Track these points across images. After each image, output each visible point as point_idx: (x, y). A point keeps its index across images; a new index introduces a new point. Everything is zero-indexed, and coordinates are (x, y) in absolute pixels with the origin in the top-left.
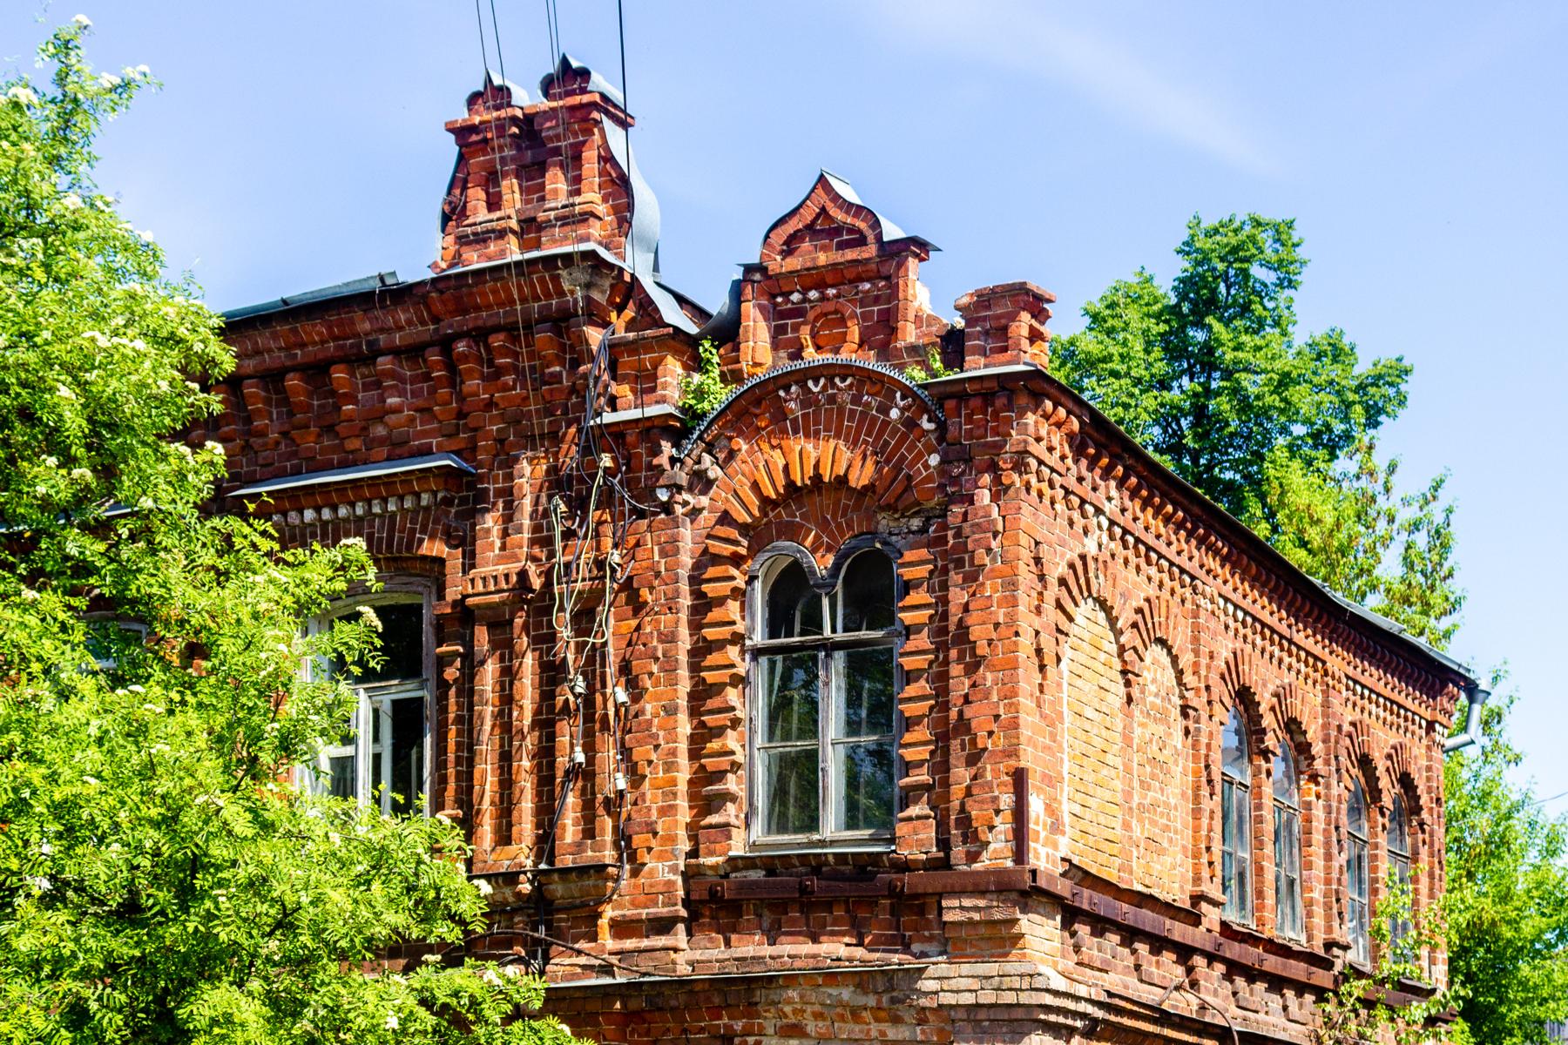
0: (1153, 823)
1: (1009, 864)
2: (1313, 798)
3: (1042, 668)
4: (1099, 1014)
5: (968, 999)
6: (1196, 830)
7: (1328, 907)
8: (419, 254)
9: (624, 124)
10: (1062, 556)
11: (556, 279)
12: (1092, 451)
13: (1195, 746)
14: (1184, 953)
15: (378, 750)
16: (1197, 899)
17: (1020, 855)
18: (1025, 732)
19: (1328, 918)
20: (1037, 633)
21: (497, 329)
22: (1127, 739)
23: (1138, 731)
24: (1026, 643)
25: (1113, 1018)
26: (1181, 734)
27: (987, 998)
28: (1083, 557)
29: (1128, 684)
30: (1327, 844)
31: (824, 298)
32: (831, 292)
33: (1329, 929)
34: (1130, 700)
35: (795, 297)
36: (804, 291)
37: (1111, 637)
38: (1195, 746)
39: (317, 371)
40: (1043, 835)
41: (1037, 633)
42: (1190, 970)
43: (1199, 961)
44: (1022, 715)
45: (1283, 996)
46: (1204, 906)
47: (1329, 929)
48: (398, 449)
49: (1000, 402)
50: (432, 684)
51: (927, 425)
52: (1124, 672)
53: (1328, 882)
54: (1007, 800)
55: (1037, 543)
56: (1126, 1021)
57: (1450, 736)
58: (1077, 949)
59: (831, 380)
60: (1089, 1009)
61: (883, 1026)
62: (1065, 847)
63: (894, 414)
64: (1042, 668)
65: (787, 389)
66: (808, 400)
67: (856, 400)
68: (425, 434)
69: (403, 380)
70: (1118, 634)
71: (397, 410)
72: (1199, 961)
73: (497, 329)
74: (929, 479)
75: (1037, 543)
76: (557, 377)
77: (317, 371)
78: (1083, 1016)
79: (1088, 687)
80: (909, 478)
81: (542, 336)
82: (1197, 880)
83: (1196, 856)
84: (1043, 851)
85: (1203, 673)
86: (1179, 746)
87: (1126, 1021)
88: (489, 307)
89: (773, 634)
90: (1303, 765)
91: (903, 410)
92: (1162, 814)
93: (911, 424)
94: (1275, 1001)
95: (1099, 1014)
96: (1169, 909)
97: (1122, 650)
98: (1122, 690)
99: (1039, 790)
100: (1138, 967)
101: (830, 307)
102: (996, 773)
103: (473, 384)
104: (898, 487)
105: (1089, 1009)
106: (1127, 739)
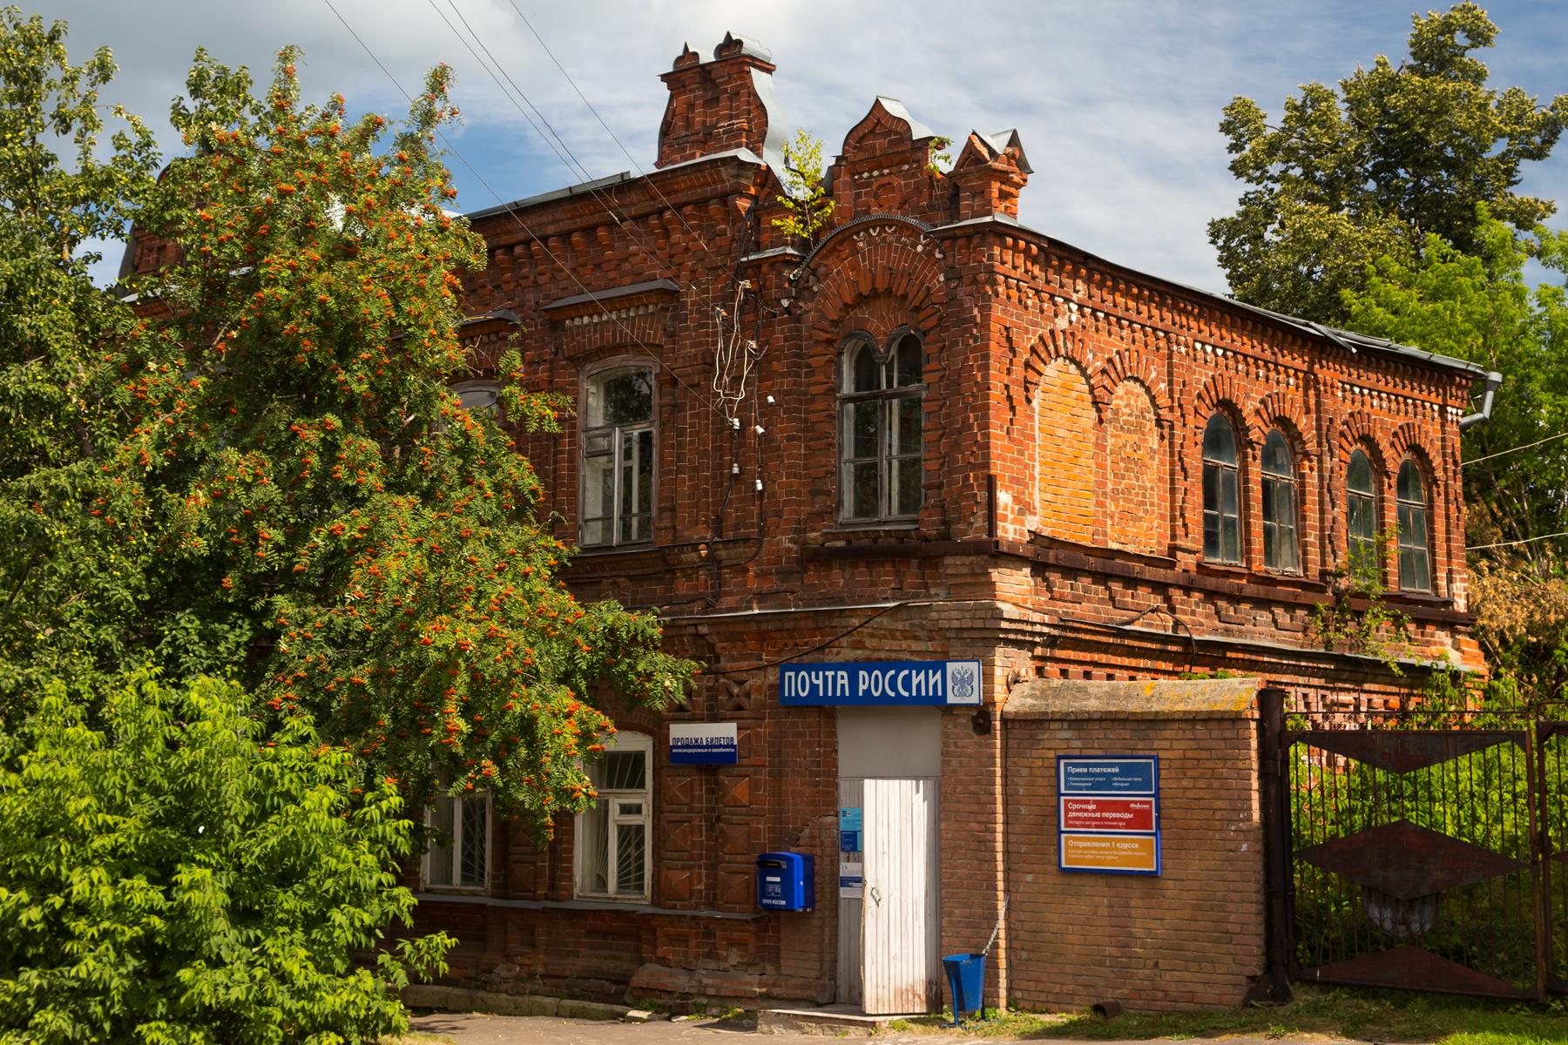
0: (1127, 500)
1: (985, 537)
2: (1307, 471)
3: (1013, 409)
4: (1056, 632)
5: (956, 624)
6: (1173, 501)
7: (1322, 547)
8: (642, 160)
9: (768, 69)
10: (1034, 333)
11: (718, 173)
12: (1056, 263)
13: (1171, 444)
14: (1160, 588)
15: (629, 463)
16: (1173, 549)
17: (992, 529)
18: (994, 451)
19: (1323, 554)
20: (1007, 387)
21: (688, 203)
22: (1101, 447)
23: (1110, 441)
24: (996, 393)
25: (1070, 635)
26: (1156, 439)
27: (966, 624)
28: (1052, 332)
29: (1099, 410)
30: (1321, 502)
31: (881, 175)
32: (886, 171)
33: (1323, 563)
34: (1101, 421)
35: (866, 175)
36: (870, 172)
37: (1083, 380)
38: (1171, 444)
39: (589, 231)
40: (1010, 516)
41: (1007, 387)
42: (1168, 599)
43: (1177, 595)
44: (992, 441)
45: (1272, 613)
46: (1179, 554)
47: (1323, 563)
48: (638, 276)
49: (976, 240)
50: (657, 423)
51: (938, 256)
52: (1095, 403)
53: (1322, 529)
54: (982, 496)
55: (1007, 329)
56: (1082, 636)
57: (1464, 415)
58: (1049, 589)
59: (882, 227)
60: (1046, 630)
61: (909, 642)
62: (1033, 523)
63: (920, 248)
64: (1013, 409)
65: (858, 234)
66: (870, 241)
67: (898, 240)
68: (652, 267)
69: (640, 236)
70: (1088, 378)
71: (635, 254)
72: (1177, 595)
73: (688, 203)
74: (940, 289)
75: (1007, 329)
76: (723, 233)
77: (589, 231)
78: (1041, 634)
79: (1060, 416)
80: (928, 289)
81: (714, 206)
82: (1173, 537)
83: (1173, 519)
84: (1010, 528)
85: (1176, 396)
86: (1155, 447)
87: (1082, 636)
88: (702, 186)
89: (857, 389)
90: (1298, 449)
91: (925, 246)
92: (1137, 495)
93: (930, 254)
94: (1264, 616)
95: (1056, 632)
96: (1150, 561)
97: (1092, 389)
98: (1094, 414)
99: (1007, 488)
100: (1112, 599)
101: (885, 180)
102: (976, 478)
103: (675, 237)
104: (921, 295)
105: (1046, 630)
106: (1101, 447)
